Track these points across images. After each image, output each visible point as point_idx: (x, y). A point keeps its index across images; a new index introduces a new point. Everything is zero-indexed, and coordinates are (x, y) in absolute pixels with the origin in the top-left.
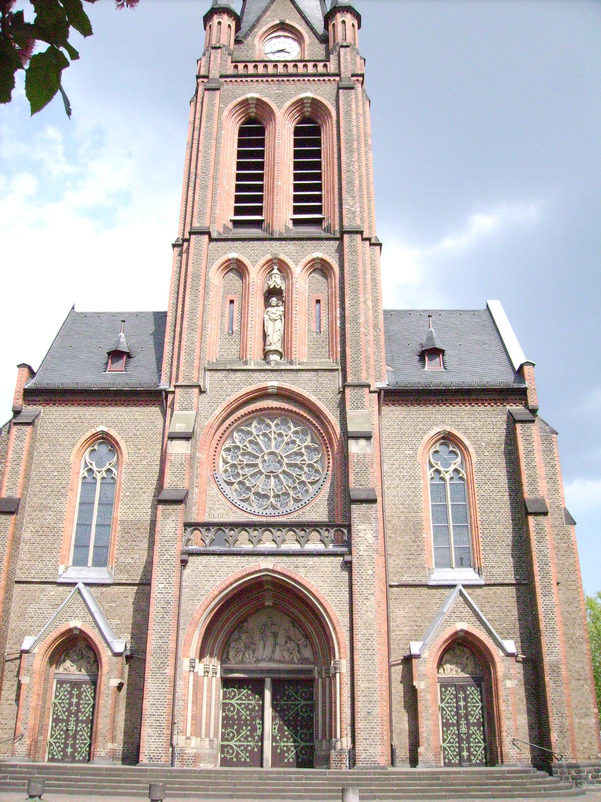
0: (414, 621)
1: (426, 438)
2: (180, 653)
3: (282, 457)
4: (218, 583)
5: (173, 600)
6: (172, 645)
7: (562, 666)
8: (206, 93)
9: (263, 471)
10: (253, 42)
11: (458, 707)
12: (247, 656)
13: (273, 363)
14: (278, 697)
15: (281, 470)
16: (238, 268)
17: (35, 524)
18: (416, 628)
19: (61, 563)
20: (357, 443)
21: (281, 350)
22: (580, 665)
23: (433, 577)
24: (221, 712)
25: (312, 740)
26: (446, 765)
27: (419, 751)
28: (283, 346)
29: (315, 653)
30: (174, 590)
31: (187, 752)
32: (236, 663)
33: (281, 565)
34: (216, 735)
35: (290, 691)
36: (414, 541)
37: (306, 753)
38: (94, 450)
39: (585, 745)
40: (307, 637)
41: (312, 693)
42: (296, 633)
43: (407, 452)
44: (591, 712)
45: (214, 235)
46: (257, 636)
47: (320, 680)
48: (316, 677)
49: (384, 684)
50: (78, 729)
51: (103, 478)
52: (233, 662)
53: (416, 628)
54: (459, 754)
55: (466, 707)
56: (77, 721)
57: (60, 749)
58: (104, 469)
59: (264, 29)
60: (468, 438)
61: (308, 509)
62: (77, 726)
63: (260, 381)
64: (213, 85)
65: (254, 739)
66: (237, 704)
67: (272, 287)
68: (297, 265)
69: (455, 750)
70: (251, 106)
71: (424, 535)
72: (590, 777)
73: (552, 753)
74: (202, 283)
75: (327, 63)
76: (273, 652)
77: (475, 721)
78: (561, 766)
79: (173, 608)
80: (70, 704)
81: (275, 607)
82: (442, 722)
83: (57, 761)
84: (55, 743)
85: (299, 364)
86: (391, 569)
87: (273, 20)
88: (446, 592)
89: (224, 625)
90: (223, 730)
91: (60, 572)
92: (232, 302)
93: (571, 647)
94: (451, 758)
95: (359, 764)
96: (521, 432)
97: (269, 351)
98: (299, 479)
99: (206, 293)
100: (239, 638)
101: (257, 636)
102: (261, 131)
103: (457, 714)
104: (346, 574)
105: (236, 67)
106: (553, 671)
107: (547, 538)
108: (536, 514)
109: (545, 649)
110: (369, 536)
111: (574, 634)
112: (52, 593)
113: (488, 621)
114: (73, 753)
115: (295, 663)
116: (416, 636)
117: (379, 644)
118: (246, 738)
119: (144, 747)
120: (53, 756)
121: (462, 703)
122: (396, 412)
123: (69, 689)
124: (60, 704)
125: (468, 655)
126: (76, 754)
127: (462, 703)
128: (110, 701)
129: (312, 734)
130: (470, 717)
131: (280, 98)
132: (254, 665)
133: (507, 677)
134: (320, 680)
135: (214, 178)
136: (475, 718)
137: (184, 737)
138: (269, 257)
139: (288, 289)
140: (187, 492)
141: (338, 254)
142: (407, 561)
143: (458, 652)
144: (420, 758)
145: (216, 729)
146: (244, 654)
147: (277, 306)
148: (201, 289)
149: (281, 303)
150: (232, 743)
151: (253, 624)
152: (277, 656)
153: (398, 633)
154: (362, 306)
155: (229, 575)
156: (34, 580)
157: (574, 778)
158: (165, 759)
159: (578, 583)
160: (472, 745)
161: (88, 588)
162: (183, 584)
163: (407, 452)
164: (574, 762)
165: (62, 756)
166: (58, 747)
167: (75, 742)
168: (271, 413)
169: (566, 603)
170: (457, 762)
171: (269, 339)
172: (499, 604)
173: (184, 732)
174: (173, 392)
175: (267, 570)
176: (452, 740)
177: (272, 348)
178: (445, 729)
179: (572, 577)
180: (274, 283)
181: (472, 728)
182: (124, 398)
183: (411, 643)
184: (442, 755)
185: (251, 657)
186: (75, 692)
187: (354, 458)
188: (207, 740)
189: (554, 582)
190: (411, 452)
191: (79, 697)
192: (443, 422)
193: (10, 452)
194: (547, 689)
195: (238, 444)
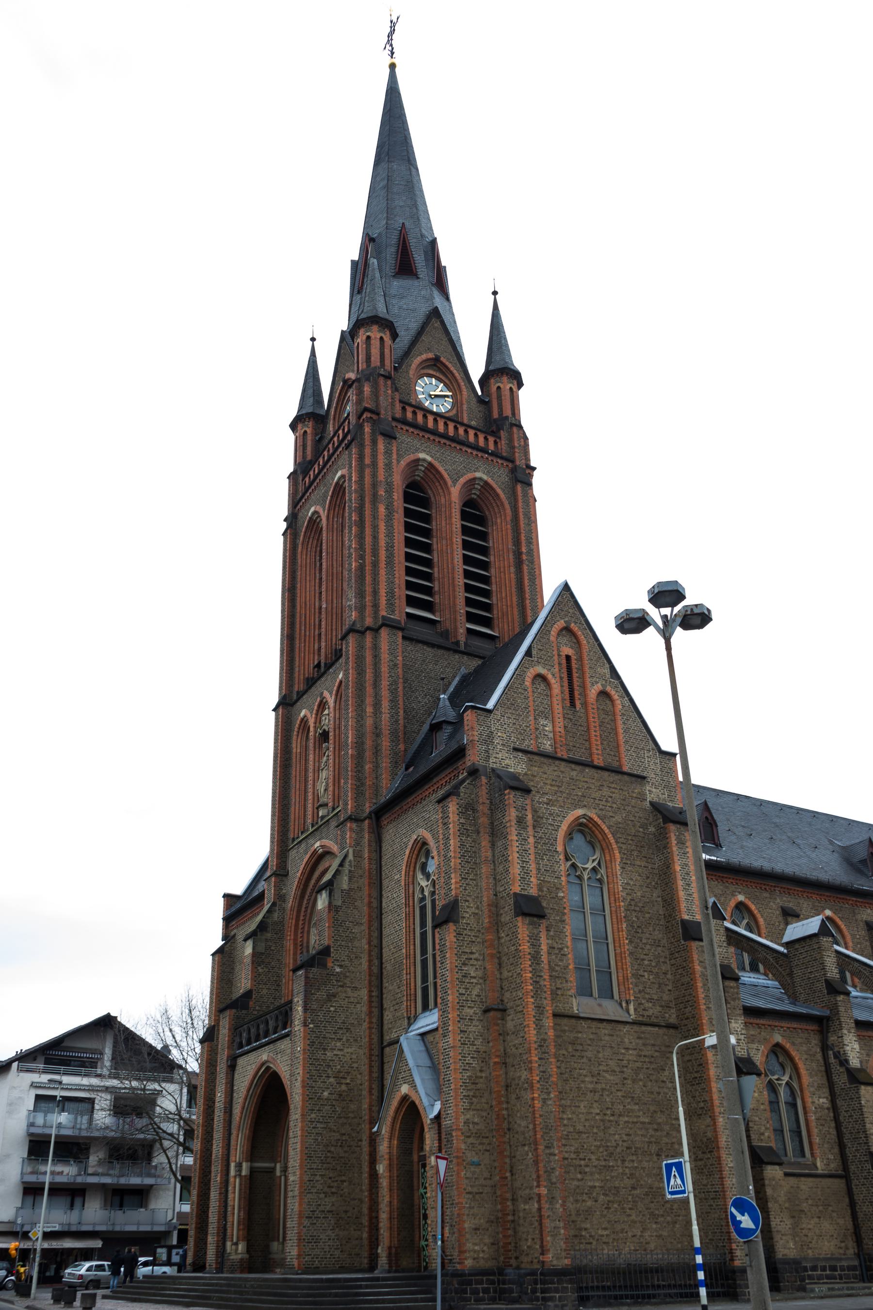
31: (232, 1257)
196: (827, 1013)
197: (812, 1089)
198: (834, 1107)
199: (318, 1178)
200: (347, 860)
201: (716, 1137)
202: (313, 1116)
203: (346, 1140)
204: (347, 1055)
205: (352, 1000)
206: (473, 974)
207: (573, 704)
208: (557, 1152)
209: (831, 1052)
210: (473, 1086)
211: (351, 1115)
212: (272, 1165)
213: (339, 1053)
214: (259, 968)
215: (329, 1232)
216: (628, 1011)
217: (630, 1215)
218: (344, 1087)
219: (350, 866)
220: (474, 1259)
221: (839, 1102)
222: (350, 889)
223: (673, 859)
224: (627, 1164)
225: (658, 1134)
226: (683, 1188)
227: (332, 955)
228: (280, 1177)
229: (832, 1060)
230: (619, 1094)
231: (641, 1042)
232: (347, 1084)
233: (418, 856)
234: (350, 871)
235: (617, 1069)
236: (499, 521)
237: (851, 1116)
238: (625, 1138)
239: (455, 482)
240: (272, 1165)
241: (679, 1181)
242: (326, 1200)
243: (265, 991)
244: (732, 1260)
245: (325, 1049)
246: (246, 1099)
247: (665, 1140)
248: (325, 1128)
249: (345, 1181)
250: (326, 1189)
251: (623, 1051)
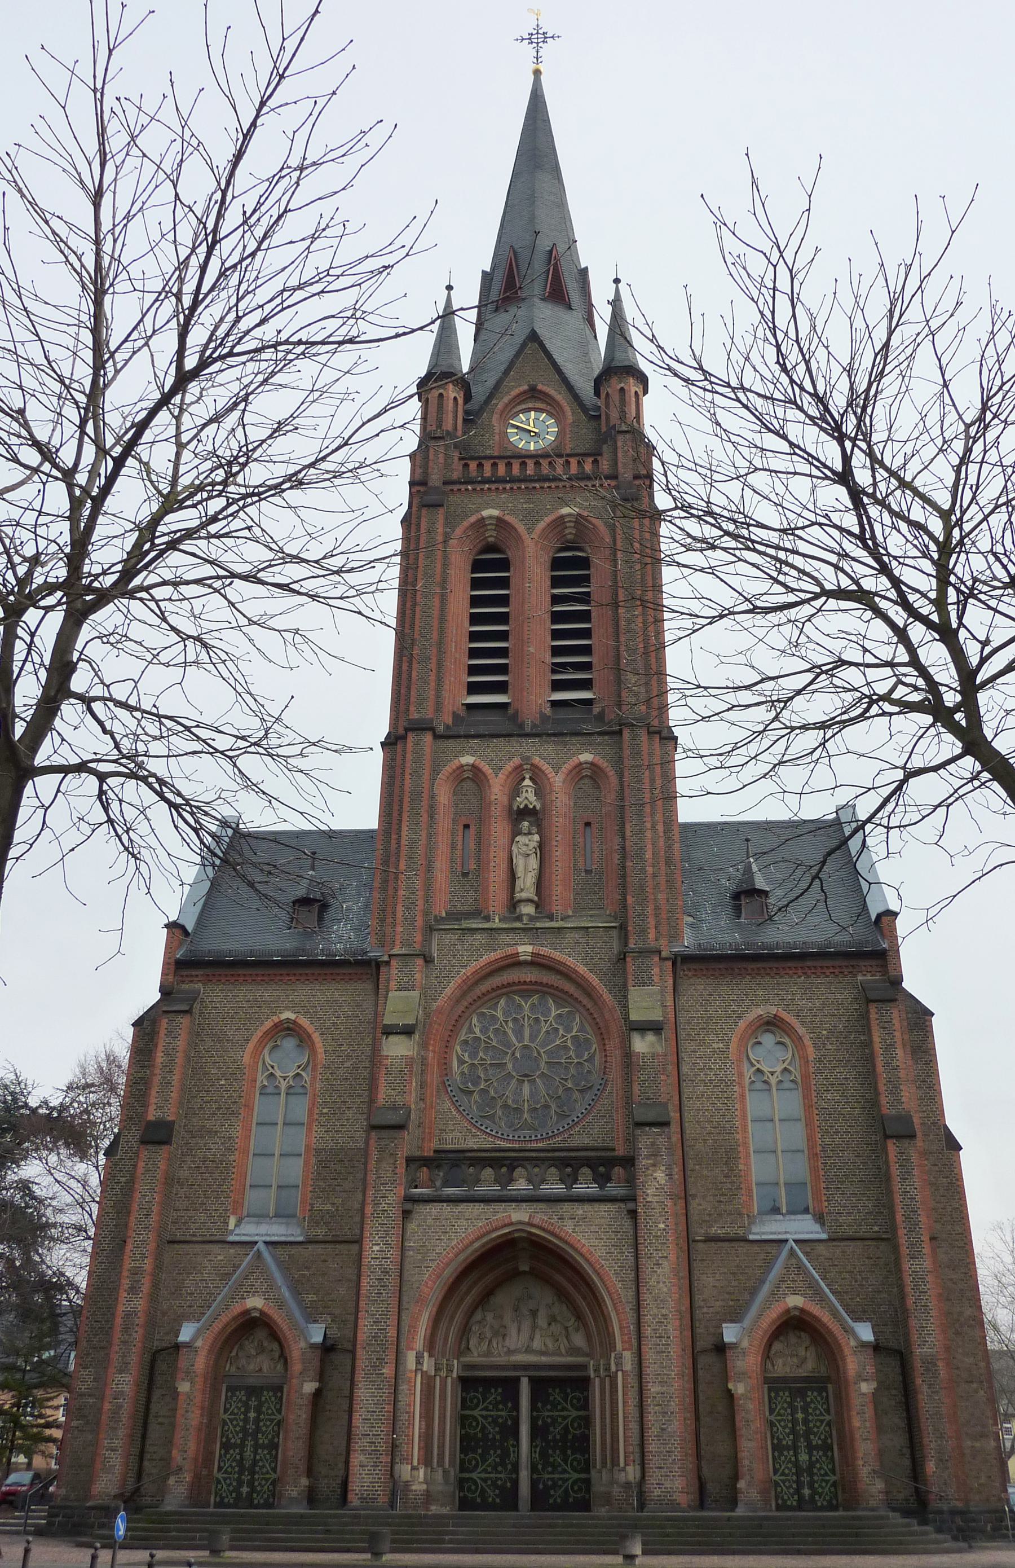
0: (729, 1293)
1: (742, 1024)
2: (403, 1344)
3: (539, 1053)
4: (454, 1243)
5: (393, 1267)
6: (392, 1333)
7: (940, 1364)
8: (424, 511)
9: (514, 1074)
10: (490, 421)
12: (495, 1345)
13: (525, 919)
14: (540, 1405)
15: (538, 1073)
16: (476, 776)
17: (194, 1156)
18: (731, 1303)
19: (233, 1213)
20: (643, 1037)
21: (536, 898)
22: (971, 1360)
23: (755, 1229)
24: (459, 1428)
25: (587, 1469)
26: (779, 1508)
27: (738, 1486)
28: (538, 893)
29: (589, 1338)
30: (393, 1254)
31: (414, 1488)
32: (479, 1356)
33: (539, 1215)
34: (452, 1463)
35: (556, 1395)
37: (580, 1489)
38: (277, 1046)
39: (982, 1481)
40: (579, 1317)
41: (586, 1399)
42: (560, 1310)
45: (441, 729)
46: (508, 1316)
47: (597, 1380)
48: (592, 1375)
49: (687, 1386)
50: (258, 1457)
51: (291, 1087)
52: (476, 1354)
53: (731, 1303)
54: (798, 1491)
55: (806, 1422)
56: (256, 1446)
57: (231, 1488)
58: (291, 1074)
59: (506, 399)
60: (803, 1023)
61: (577, 1129)
62: (255, 1453)
63: (508, 945)
64: (431, 498)
65: (506, 1469)
66: (482, 1416)
67: (522, 807)
68: (557, 773)
69: (791, 1486)
71: (741, 1167)
72: (989, 1528)
73: (928, 1492)
74: (425, 803)
75: (599, 458)
76: (532, 1339)
77: (820, 1442)
78: (941, 1512)
79: (392, 1280)
80: (246, 1420)
81: (533, 1273)
82: (772, 1443)
83: (228, 1506)
84: (225, 1479)
85: (562, 920)
86: (694, 1217)
87: (520, 385)
88: (772, 1249)
89: (462, 1299)
90: (462, 1456)
91: (231, 1226)
92: (466, 826)
93: (957, 1333)
94: (786, 1497)
95: (651, 1506)
96: (877, 1016)
97: (520, 901)
98: (564, 1085)
99: (432, 817)
100: (484, 1319)
101: (508, 1316)
102: (504, 564)
103: (793, 1431)
104: (627, 1223)
105: (466, 465)
106: (928, 1370)
107: (915, 1172)
108: (898, 1137)
109: (914, 1337)
110: (660, 1175)
111: (960, 1313)
112: (220, 1258)
113: (833, 1293)
114: (250, 1494)
115: (561, 1355)
116: (735, 1316)
117: (673, 1330)
118: (495, 1468)
119: (354, 1482)
120: (222, 1498)
121: (800, 1416)
122: (698, 987)
123: (244, 1398)
124: (231, 1421)
125: (808, 1343)
126: (255, 1495)
127: (800, 1416)
128: (304, 1416)
129: (587, 1462)
130: (812, 1437)
131: (530, 518)
132: (506, 1358)
133: (861, 1378)
134: (597, 1380)
135: (440, 643)
136: (819, 1438)
137: (409, 1467)
138: (517, 761)
139: (543, 806)
140: (425, 1162)
142: (716, 1204)
143: (793, 1339)
144: (741, 1497)
145: (452, 1455)
146: (490, 1341)
147: (529, 833)
148: (423, 812)
149: (534, 830)
150: (474, 1475)
151: (502, 1298)
152: (537, 1344)
153: (705, 1310)
154: (649, 834)
155: (470, 1231)
156: (194, 1239)
157: (960, 1530)
158: (383, 1499)
160: (816, 1478)
161: (270, 1248)
162: (406, 1244)
163: (715, 1046)
164: (959, 1505)
165: (235, 1499)
166: (229, 1485)
167: (253, 1478)
168: (526, 990)
170: (795, 1503)
171: (519, 883)
172: (849, 1268)
173: (409, 1460)
174: (388, 963)
175: (520, 1223)
176: (787, 1471)
177: (524, 895)
178: (776, 1454)
179: (957, 1228)
180: (526, 802)
181: (815, 1453)
182: (317, 971)
183: (724, 1325)
184: (773, 1493)
185: (500, 1346)
186: (253, 1403)
187: (638, 1059)
188: (440, 1471)
189: (925, 1238)
190: (721, 1045)
191: (258, 1410)
192: (767, 1001)
193: (159, 1054)
194: (920, 1397)
195: (478, 1034)
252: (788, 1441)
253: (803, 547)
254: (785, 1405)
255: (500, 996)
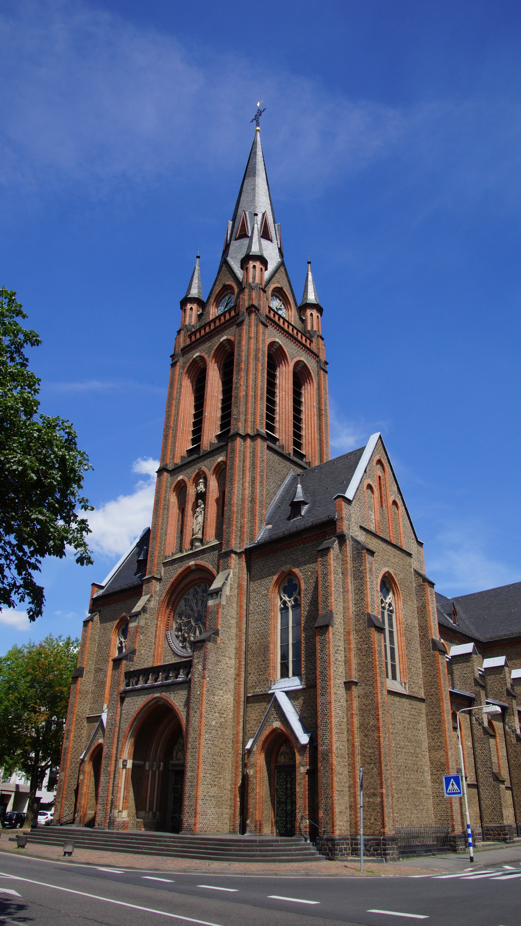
11: (286, 788)
31: (118, 820)
36: (264, 661)
39: (372, 821)
43: (263, 592)
44: (378, 792)
70: (226, 345)
103: (286, 794)
141: (47, 556)
153: (251, 732)
159: (374, 678)
169: (364, 697)
188: (151, 813)
196: (473, 696)
197: (466, 737)
198: (474, 747)
199: (208, 775)
200: (229, 577)
201: (448, 763)
202: (207, 736)
203: (223, 753)
204: (225, 699)
205: (229, 665)
206: (340, 659)
207: (382, 506)
208: (389, 768)
209: (474, 718)
210: (340, 727)
211: (226, 737)
212: (143, 763)
213: (221, 698)
214: (141, 636)
215: (213, 809)
216: (405, 688)
217: (406, 805)
218: (223, 720)
219: (231, 581)
220: (340, 830)
221: (476, 745)
222: (231, 596)
223: (428, 604)
224: (405, 776)
225: (417, 759)
226: (459, 791)
227: (220, 635)
228: (149, 770)
229: (474, 722)
230: (402, 736)
231: (410, 706)
232: (225, 718)
233: (282, 581)
234: (231, 584)
235: (402, 722)
236: (309, 388)
237: (483, 753)
238: (405, 761)
239: (292, 359)
240: (143, 763)
241: (456, 787)
242: (212, 789)
243: (143, 651)
244: (453, 830)
245: (214, 695)
246: (135, 719)
247: (419, 763)
248: (212, 744)
249: (221, 778)
250: (212, 782)
251: (404, 711)
252: (283, 800)
253: (253, 329)
254: (283, 780)
255: (189, 588)
